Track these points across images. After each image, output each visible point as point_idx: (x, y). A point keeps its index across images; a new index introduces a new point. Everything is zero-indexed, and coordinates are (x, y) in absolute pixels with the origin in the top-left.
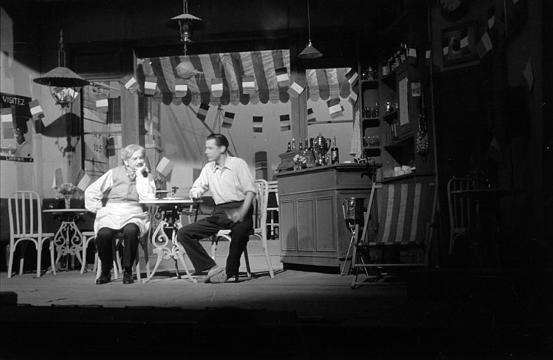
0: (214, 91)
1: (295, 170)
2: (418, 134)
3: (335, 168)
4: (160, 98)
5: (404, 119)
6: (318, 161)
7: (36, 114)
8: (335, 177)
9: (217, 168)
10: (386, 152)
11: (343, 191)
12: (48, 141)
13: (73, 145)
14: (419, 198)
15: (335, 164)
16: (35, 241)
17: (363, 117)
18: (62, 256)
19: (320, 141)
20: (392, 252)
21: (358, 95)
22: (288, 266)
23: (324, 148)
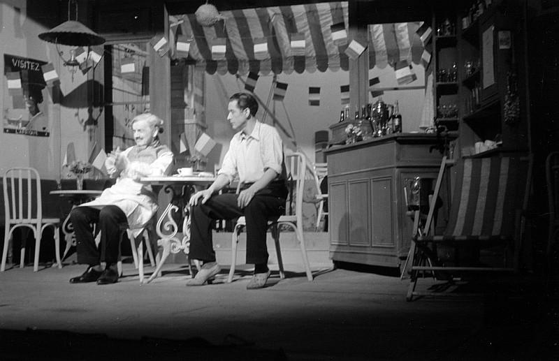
0: (257, 53)
1: (347, 144)
2: (506, 96)
3: (395, 138)
4: (202, 67)
5: (488, 79)
6: (377, 133)
7: (50, 80)
8: (395, 150)
9: (243, 138)
10: (466, 125)
11: (407, 169)
12: (68, 113)
13: (95, 118)
14: (506, 176)
15: (396, 135)
16: (34, 228)
17: (437, 81)
18: (171, 254)
19: (379, 107)
20: (466, 250)
21: (432, 54)
22: (339, 265)
23: (385, 117)
